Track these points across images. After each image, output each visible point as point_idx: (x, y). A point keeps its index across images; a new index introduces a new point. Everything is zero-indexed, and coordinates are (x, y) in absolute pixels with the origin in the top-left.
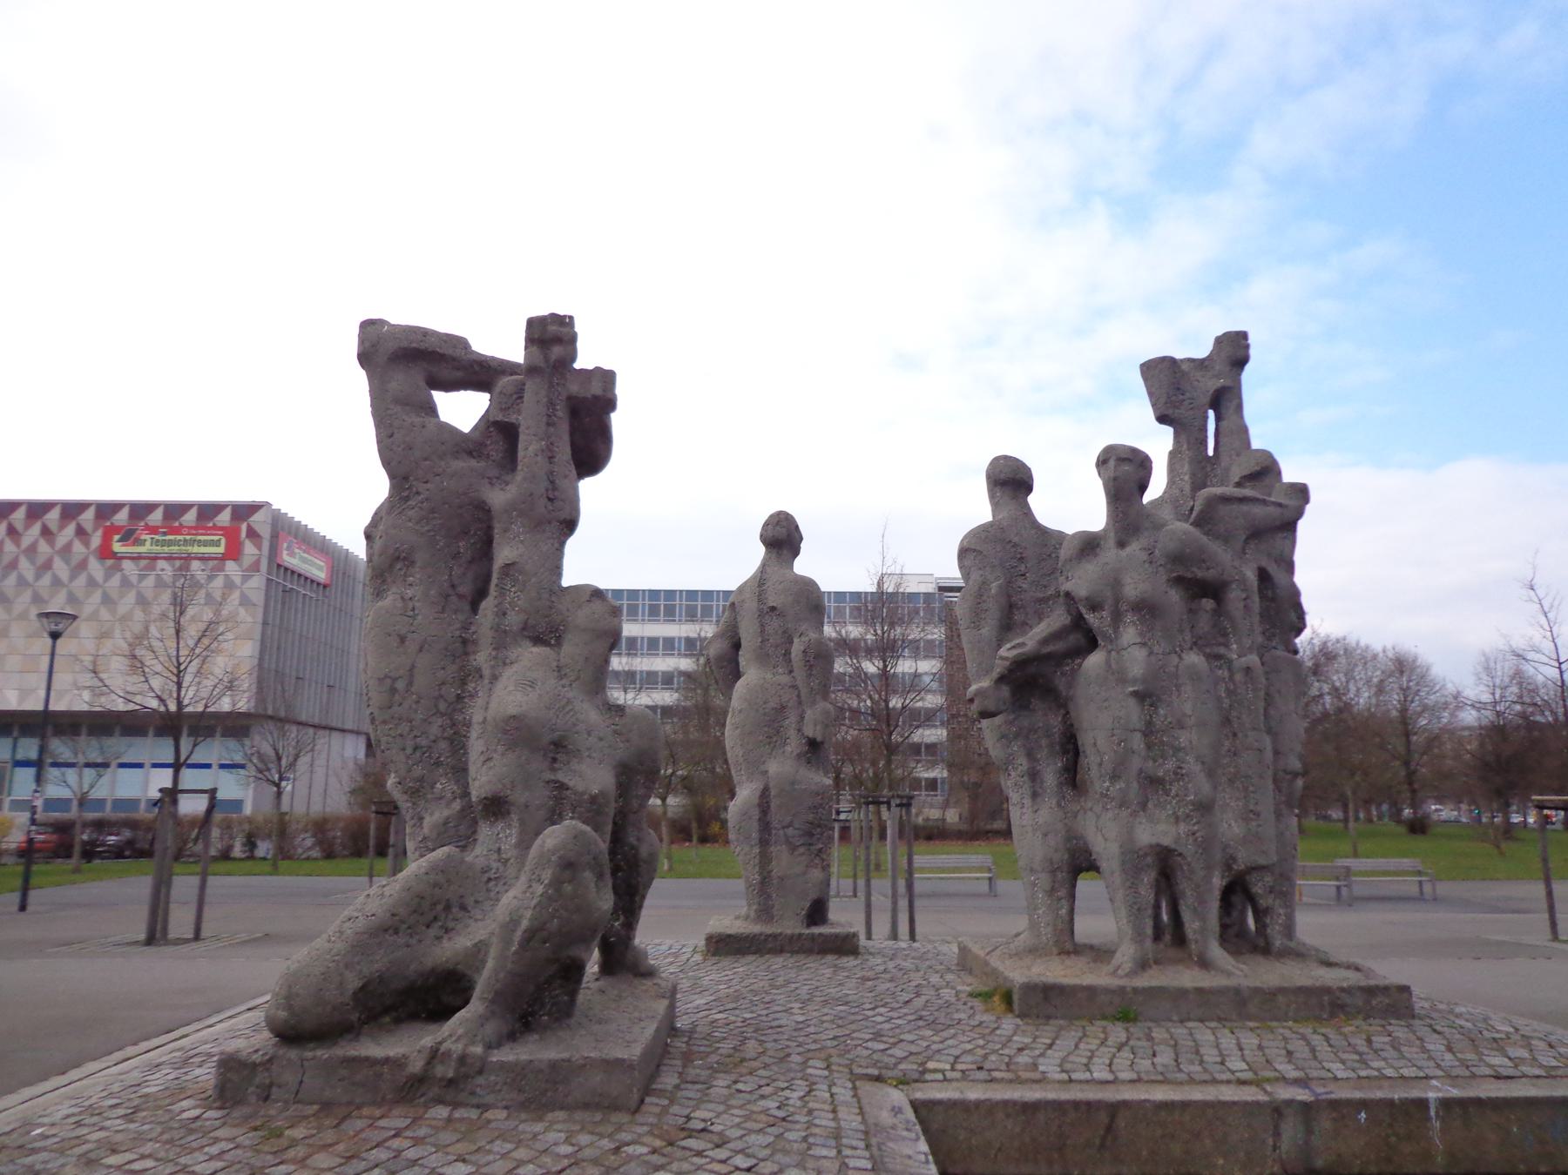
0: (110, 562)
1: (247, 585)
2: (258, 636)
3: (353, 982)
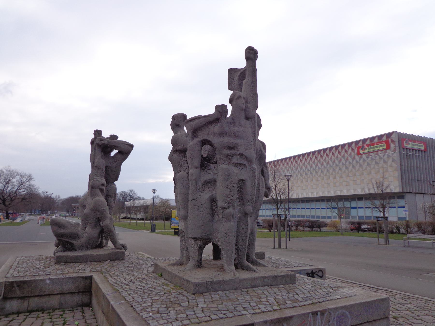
0: (360, 156)
1: (394, 156)
2: (399, 170)
3: (251, 256)
